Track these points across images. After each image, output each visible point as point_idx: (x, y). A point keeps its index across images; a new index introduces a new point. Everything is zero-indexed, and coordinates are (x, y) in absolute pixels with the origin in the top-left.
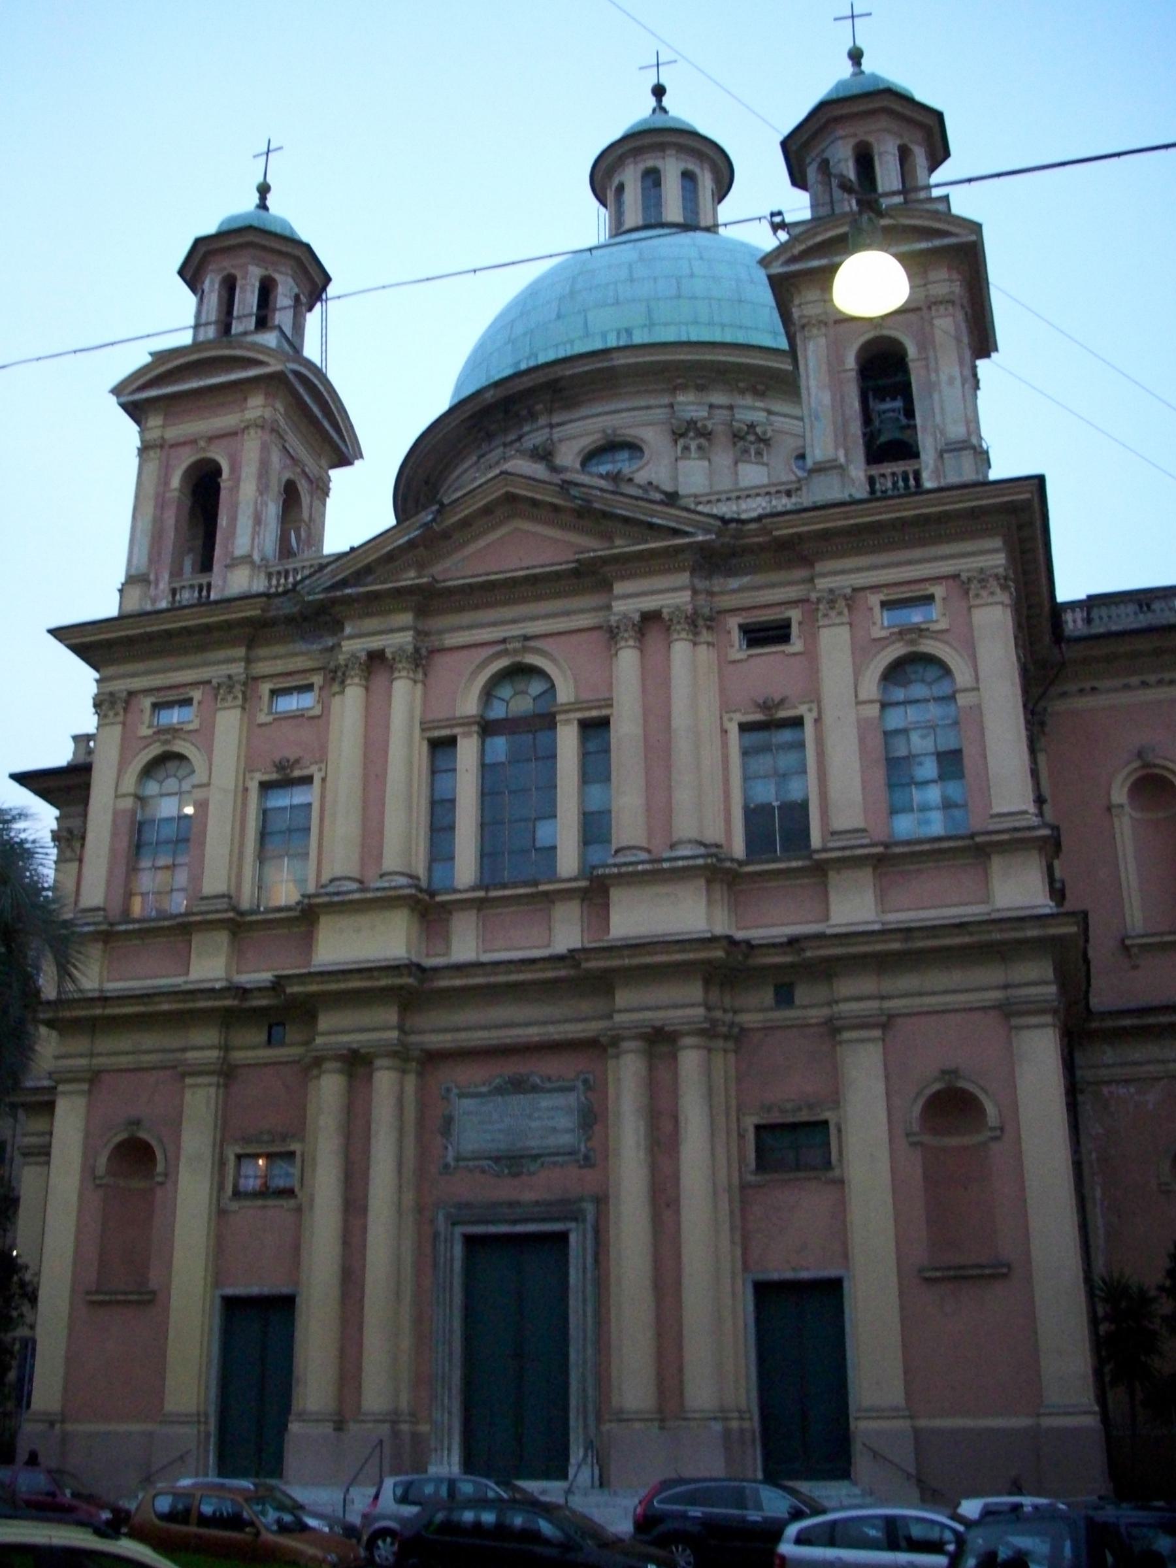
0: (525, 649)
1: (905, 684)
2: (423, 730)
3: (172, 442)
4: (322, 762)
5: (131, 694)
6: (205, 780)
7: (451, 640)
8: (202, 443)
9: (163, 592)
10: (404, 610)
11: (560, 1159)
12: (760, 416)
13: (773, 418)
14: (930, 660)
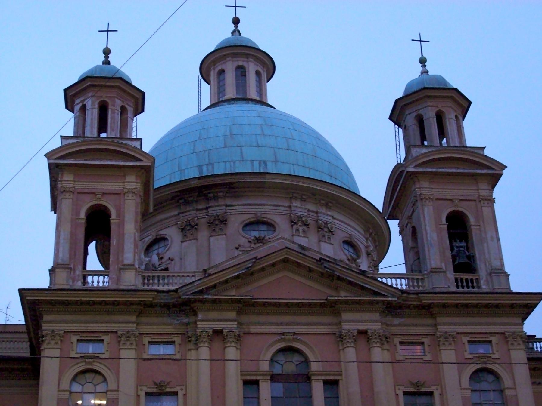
0: (294, 340)
3: (79, 191)
6: (115, 388)
7: (253, 329)
9: (79, 275)
10: (232, 310)
12: (329, 219)
14: (491, 372)
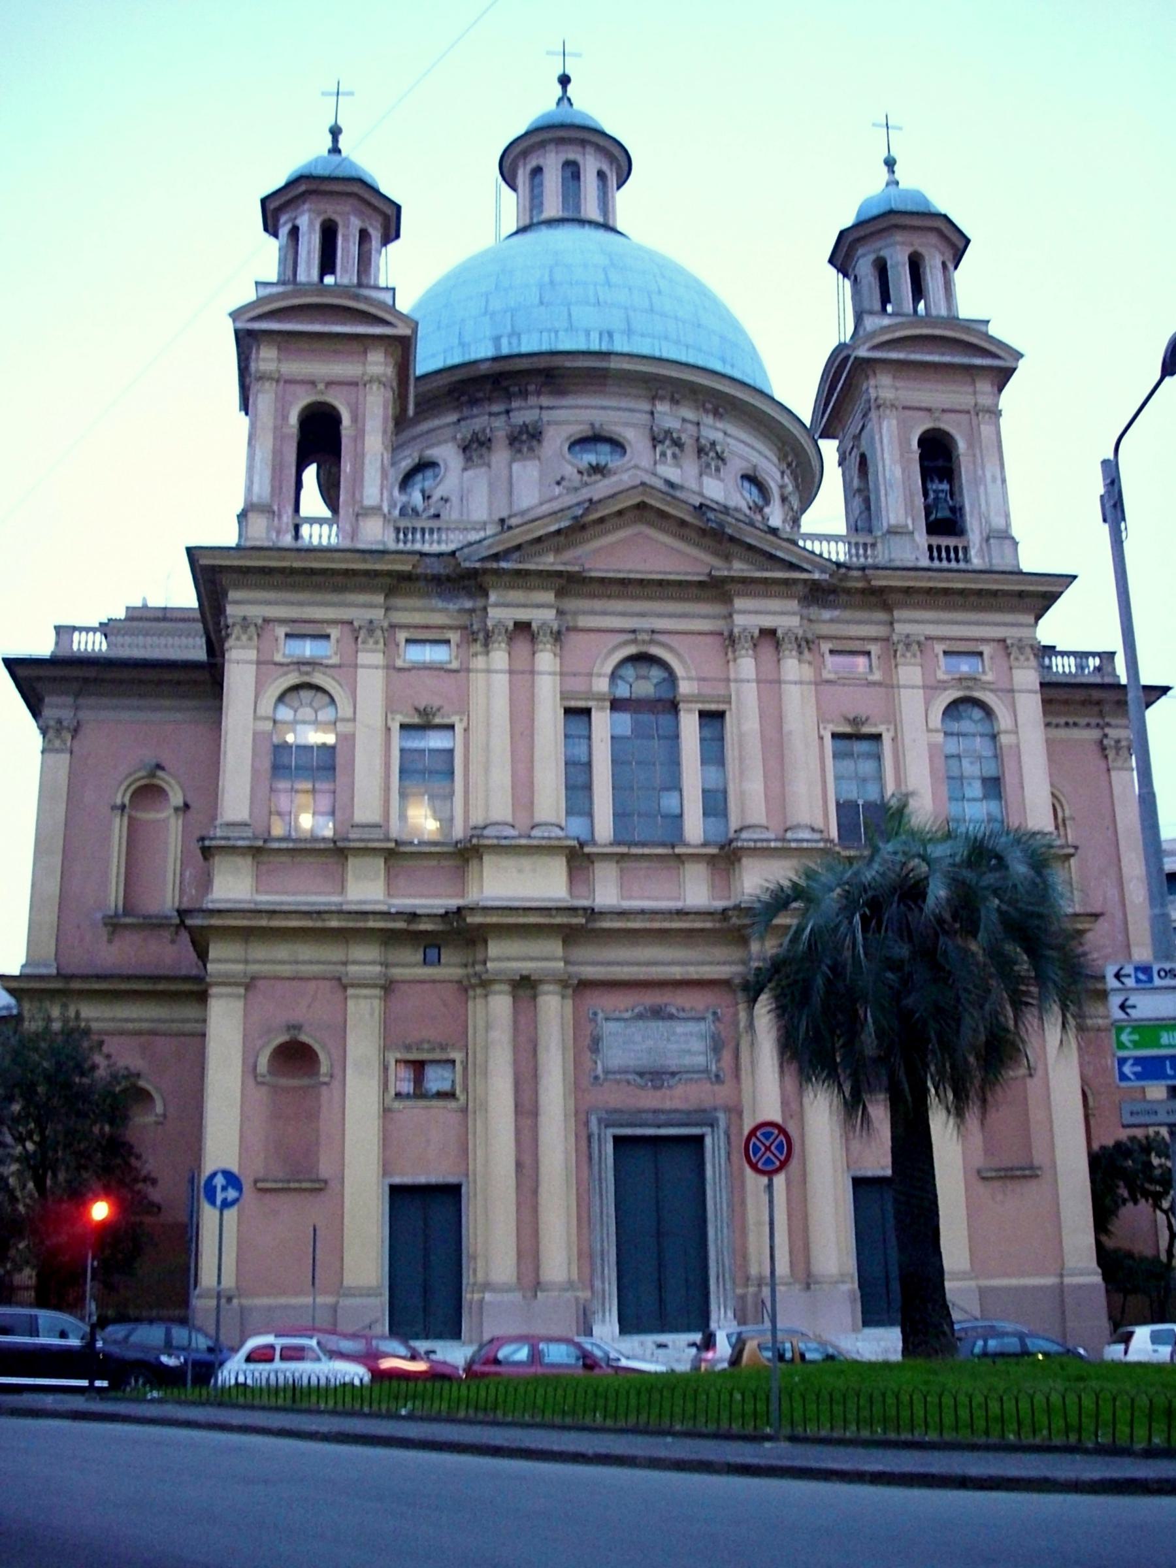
0: (652, 642)
1: (958, 718)
2: (562, 699)
4: (463, 713)
5: (266, 621)
8: (321, 386)
10: (545, 589)
11: (696, 1076)
12: (718, 436)
13: (729, 440)
